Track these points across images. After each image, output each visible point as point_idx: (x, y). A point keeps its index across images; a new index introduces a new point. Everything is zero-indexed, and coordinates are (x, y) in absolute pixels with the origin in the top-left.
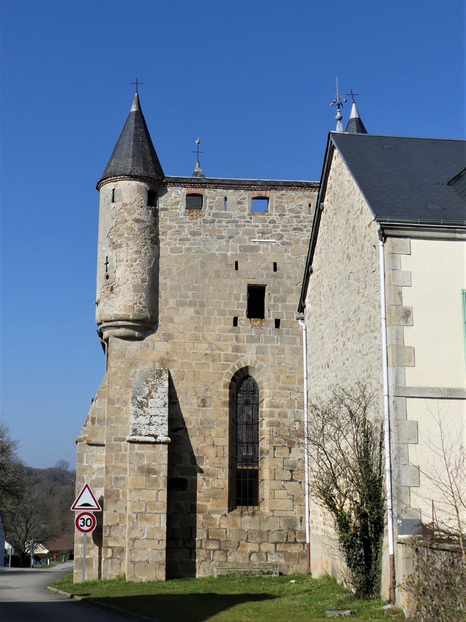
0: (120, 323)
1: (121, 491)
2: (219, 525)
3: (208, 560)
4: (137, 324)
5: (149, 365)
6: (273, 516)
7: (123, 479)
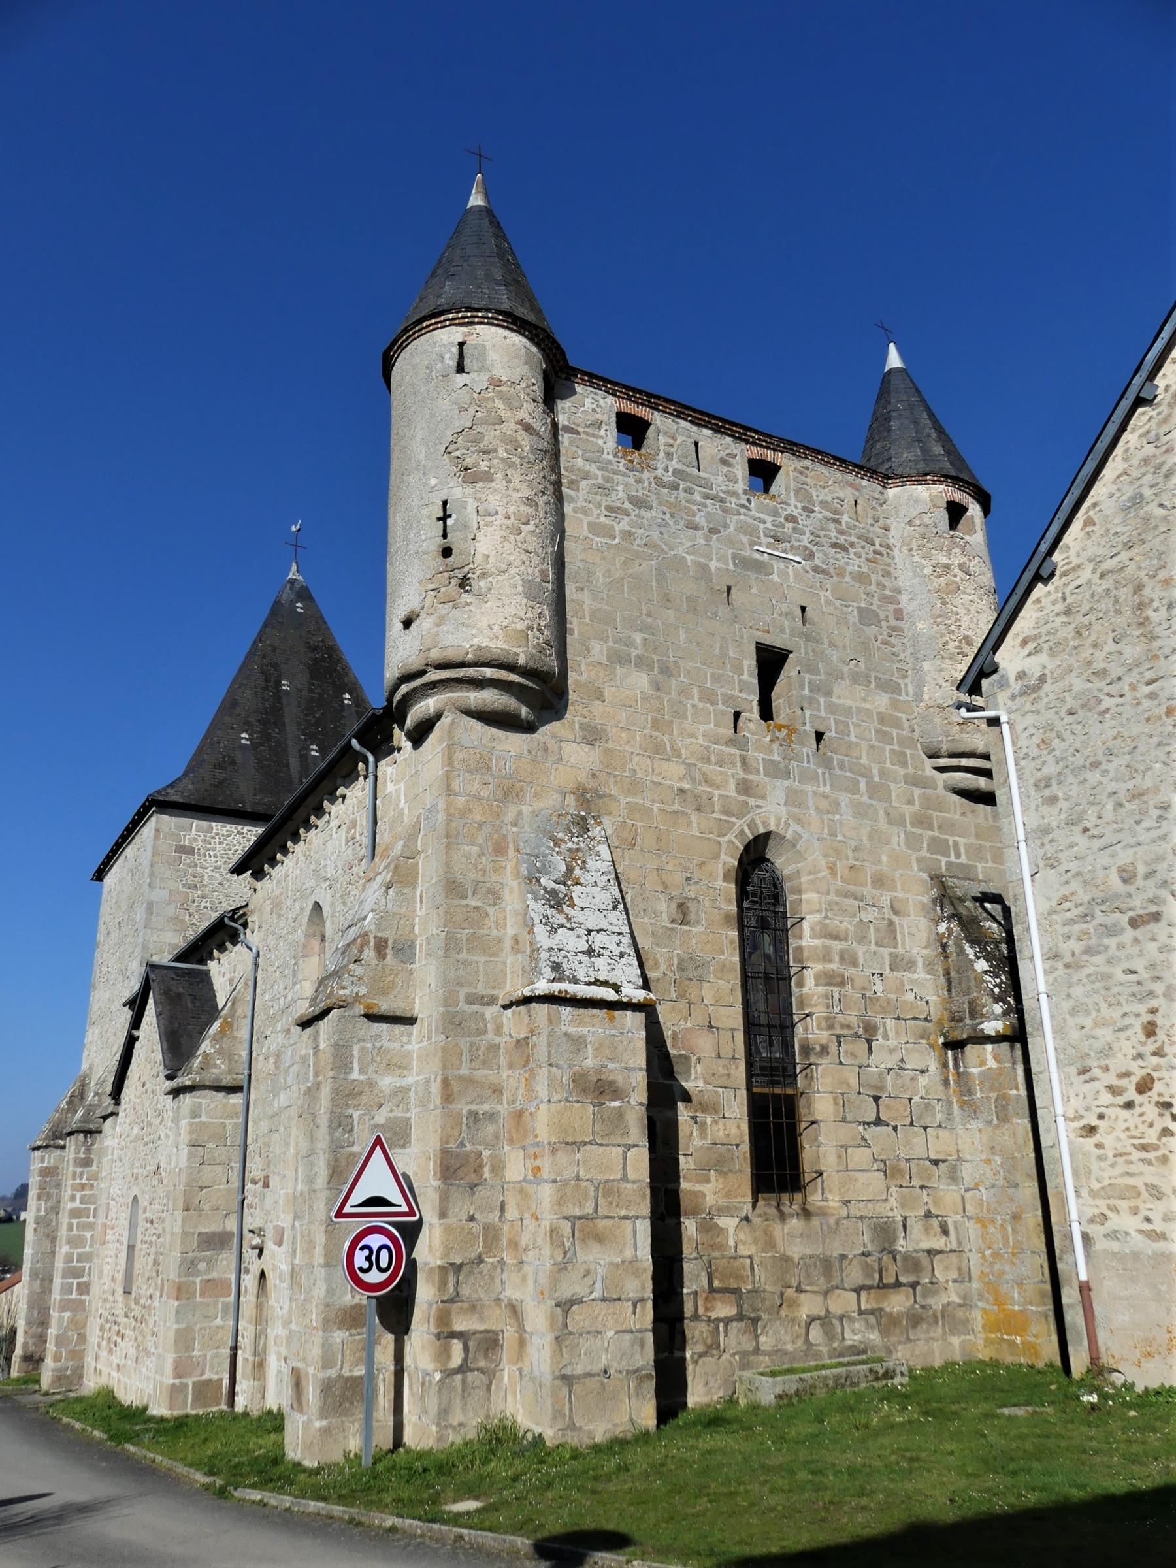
0: (488, 672)
1: (486, 1153)
2: (736, 1248)
3: (715, 1352)
4: (531, 684)
5: (552, 801)
6: (848, 1217)
7: (491, 1117)
